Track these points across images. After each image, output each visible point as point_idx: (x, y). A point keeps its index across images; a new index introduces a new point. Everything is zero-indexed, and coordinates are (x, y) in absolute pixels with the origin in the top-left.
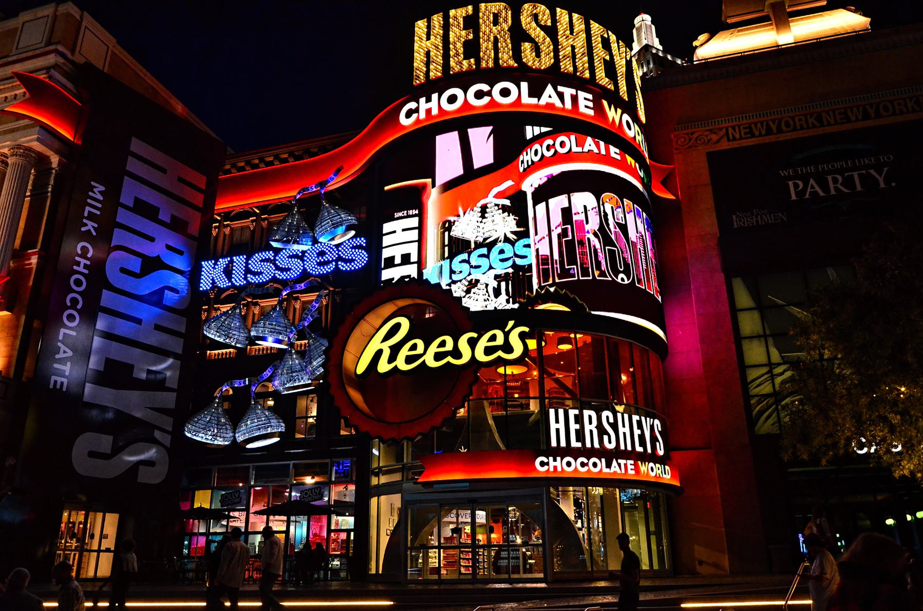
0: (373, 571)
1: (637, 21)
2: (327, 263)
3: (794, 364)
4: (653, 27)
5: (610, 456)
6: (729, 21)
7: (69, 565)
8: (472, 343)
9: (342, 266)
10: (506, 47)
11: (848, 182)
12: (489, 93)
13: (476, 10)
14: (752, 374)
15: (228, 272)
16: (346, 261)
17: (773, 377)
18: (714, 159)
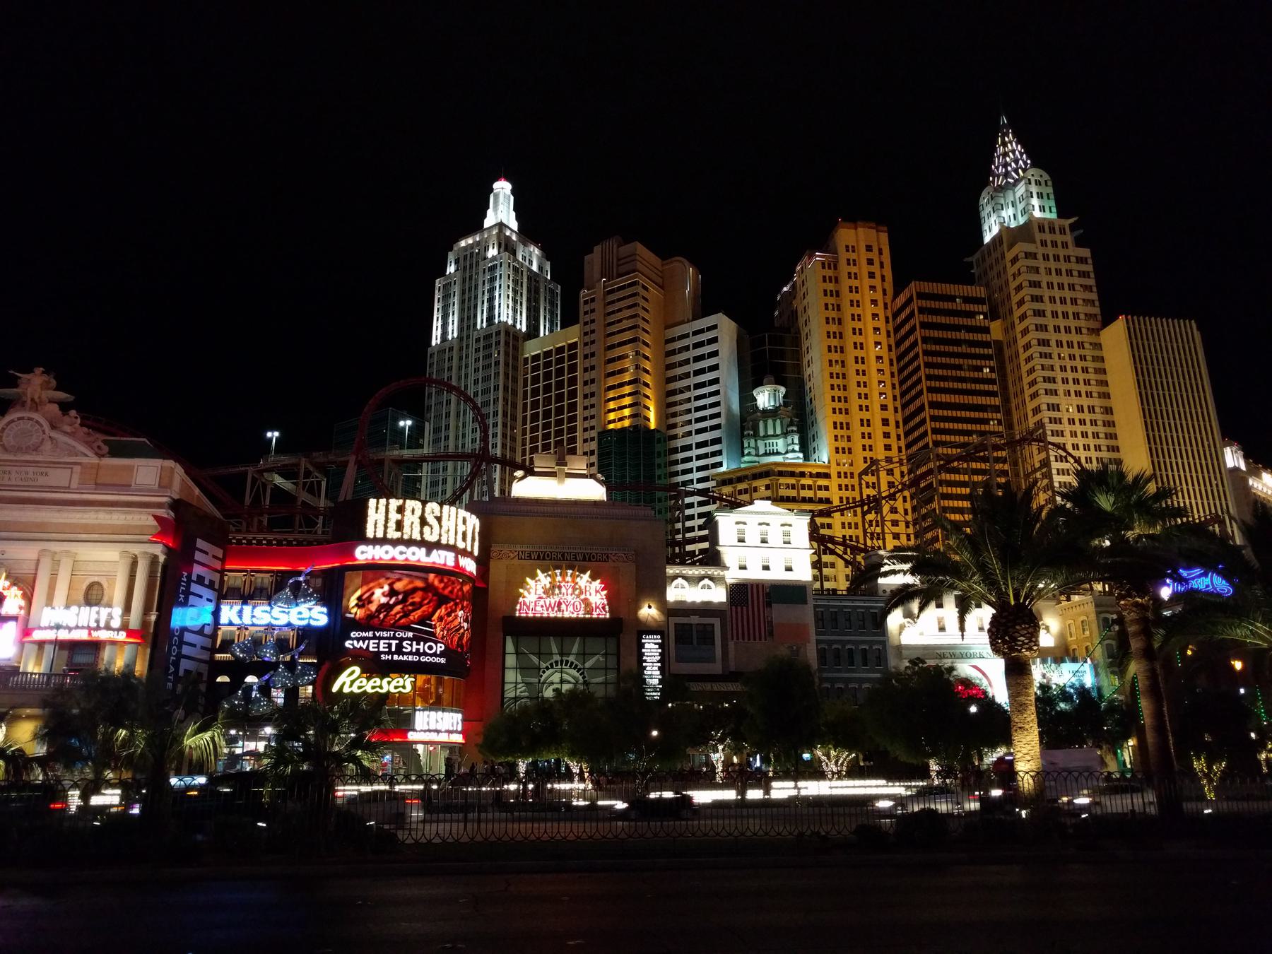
3: (527, 684)
4: (512, 198)
5: (438, 731)
6: (536, 470)
7: (897, 823)
8: (389, 683)
13: (404, 503)
14: (507, 687)
15: (240, 613)
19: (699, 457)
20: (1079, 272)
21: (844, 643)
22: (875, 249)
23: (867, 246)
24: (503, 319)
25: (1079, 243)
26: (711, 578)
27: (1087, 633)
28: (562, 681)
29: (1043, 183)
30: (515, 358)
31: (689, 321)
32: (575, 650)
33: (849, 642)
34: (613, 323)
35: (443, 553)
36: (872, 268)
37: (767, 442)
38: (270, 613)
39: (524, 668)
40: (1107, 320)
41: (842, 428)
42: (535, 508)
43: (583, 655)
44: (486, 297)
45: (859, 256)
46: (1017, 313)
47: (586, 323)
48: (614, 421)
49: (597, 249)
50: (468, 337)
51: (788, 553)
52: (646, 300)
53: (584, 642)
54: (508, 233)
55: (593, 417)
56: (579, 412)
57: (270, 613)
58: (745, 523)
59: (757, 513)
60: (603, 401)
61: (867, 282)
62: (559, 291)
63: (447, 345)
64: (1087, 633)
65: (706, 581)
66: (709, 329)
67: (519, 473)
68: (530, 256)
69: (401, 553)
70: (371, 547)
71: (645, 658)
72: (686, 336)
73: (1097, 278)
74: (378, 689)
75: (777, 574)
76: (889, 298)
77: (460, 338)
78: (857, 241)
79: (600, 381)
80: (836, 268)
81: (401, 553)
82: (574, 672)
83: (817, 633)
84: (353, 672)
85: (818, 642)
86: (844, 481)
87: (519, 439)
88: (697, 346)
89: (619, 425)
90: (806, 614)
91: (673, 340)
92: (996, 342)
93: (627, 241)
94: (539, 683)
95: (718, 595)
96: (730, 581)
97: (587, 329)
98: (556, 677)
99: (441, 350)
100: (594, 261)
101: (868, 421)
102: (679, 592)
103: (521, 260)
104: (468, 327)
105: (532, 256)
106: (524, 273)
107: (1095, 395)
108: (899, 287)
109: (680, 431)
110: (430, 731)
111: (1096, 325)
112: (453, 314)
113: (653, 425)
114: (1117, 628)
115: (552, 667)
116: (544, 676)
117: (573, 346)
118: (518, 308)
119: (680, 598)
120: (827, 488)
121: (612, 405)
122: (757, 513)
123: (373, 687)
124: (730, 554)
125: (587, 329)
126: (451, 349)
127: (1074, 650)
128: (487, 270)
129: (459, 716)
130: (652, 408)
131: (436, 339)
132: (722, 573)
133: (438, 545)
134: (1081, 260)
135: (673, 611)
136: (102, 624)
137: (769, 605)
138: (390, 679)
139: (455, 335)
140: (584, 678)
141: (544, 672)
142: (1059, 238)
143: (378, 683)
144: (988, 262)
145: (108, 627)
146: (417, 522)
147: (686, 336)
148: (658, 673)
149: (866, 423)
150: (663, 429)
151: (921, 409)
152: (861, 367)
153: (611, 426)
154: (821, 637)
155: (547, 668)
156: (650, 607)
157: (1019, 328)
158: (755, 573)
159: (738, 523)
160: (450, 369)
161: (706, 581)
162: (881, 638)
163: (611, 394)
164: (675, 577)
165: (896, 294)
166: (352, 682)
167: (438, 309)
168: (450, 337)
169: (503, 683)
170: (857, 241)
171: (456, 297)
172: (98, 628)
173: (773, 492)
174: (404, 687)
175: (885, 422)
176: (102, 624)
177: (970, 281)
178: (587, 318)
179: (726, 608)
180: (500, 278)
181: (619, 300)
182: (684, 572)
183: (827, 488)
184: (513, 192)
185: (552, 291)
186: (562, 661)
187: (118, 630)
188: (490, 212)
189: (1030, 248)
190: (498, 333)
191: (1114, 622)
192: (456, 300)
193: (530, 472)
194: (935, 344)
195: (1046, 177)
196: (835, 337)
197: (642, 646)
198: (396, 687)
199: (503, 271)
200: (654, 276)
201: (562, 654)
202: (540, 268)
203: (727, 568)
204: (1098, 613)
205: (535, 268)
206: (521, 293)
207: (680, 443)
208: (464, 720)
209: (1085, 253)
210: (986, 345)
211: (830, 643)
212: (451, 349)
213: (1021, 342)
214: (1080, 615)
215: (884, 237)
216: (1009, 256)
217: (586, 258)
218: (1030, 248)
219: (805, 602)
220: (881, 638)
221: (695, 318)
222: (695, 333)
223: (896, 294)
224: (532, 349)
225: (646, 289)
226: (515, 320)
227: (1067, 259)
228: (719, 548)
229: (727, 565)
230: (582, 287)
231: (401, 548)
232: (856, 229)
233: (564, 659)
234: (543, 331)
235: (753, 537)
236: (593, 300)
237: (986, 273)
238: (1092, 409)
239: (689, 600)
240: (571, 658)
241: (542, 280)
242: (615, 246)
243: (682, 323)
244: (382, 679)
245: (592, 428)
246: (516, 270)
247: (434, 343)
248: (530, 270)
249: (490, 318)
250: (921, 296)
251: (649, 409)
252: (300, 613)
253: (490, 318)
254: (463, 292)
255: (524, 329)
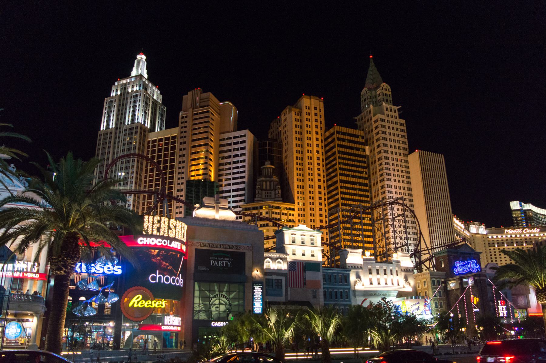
0: (330, 350)
1: (139, 56)
2: (110, 271)
3: (204, 304)
4: (146, 63)
5: (173, 326)
6: (205, 204)
8: (155, 303)
9: (115, 273)
10: (166, 231)
11: (223, 264)
12: (161, 242)
14: (195, 305)
16: (116, 271)
17: (199, 307)
18: (196, 250)
19: (234, 196)
20: (401, 129)
21: (333, 289)
22: (318, 109)
23: (315, 107)
24: (140, 121)
25: (401, 117)
26: (281, 259)
27: (426, 286)
28: (220, 304)
29: (388, 90)
30: (144, 140)
31: (232, 132)
32: (225, 289)
33: (341, 288)
34: (196, 129)
35: (176, 243)
36: (317, 118)
37: (267, 192)
38: (95, 267)
39: (204, 297)
40: (411, 151)
41: (301, 188)
42: (209, 223)
43: (229, 292)
44: (131, 110)
45: (311, 111)
46: (376, 144)
47: (182, 128)
48: (194, 176)
49: (190, 93)
50: (120, 128)
51: (313, 248)
52: (213, 120)
53: (220, 287)
54: (144, 80)
55: (183, 173)
56: (176, 170)
57: (95, 267)
58: (295, 235)
59: (301, 230)
60: (189, 166)
61: (314, 123)
62: (165, 110)
63: (109, 131)
64: (426, 286)
65: (279, 260)
66: (241, 136)
67: (197, 206)
68: (153, 92)
69: (159, 242)
70: (145, 238)
71: (255, 294)
72: (231, 138)
73: (407, 133)
74: (150, 306)
75: (308, 258)
76: (323, 132)
77: (116, 128)
78: (311, 105)
79: (188, 156)
80: (301, 115)
81: (159, 242)
82: (225, 300)
83: (324, 284)
84: (138, 297)
85: (324, 288)
86: (301, 212)
87: (143, 180)
88: (235, 143)
89: (197, 178)
90: (319, 276)
91: (224, 139)
92: (368, 155)
93: (204, 92)
94: (209, 304)
95: (284, 266)
96: (289, 260)
97: (183, 130)
98: (217, 302)
99: (106, 134)
100: (187, 99)
101: (312, 186)
102: (270, 264)
103: (149, 93)
104: (121, 123)
105: (156, 94)
106: (151, 100)
107: (405, 182)
108: (328, 126)
109: (224, 183)
110: (170, 325)
111: (407, 152)
112: (113, 116)
113: (212, 179)
114: (443, 285)
115: (215, 297)
116: (212, 301)
117: (174, 137)
118: (147, 116)
119: (279, 268)
120: (293, 215)
121: (193, 168)
122: (301, 230)
123: (148, 305)
124: (289, 249)
125: (183, 130)
126: (111, 133)
127: (420, 293)
128: (133, 97)
129: (180, 319)
130: (213, 171)
131: (103, 127)
132: (286, 256)
133: (175, 239)
134: (402, 124)
135: (267, 273)
136: (29, 270)
137: (304, 271)
138: (155, 301)
139: (114, 126)
140: (229, 302)
141: (212, 299)
142: (394, 114)
143: (150, 303)
144: (364, 120)
145: (31, 272)
146: (167, 228)
147: (231, 138)
148: (260, 301)
149: (311, 186)
150: (217, 181)
151: (336, 182)
152: (310, 161)
153: (193, 178)
154: (325, 286)
155: (213, 297)
156: (257, 271)
157: (377, 150)
158: (299, 257)
159: (292, 234)
160: (110, 142)
161: (279, 260)
162: (348, 287)
163: (193, 163)
164: (266, 258)
165: (326, 131)
166: (138, 302)
167: (105, 113)
168: (111, 127)
169: (194, 304)
170: (311, 105)
171: (115, 108)
172: (27, 272)
173: (269, 215)
174: (162, 305)
175: (320, 187)
176: (29, 270)
177: (355, 127)
178: (183, 125)
179: (287, 272)
180: (140, 101)
181: (200, 118)
182: (270, 255)
183: (293, 215)
184: (146, 60)
185: (162, 110)
186: (220, 294)
187: (36, 273)
188: (134, 69)
189: (382, 117)
190: (137, 128)
191: (443, 282)
192: (115, 109)
193: (202, 206)
194: (343, 154)
195: (389, 87)
196: (299, 147)
197: (254, 288)
198: (158, 305)
199: (141, 98)
200: (216, 109)
201: (220, 291)
202: (158, 98)
203: (289, 255)
204: (431, 278)
205: (155, 97)
206: (149, 110)
207: (224, 188)
208: (182, 321)
209: (403, 121)
210: (364, 156)
211: (328, 288)
212: (111, 133)
213: (377, 157)
214: (423, 279)
215: (322, 104)
216: (374, 119)
217: (184, 97)
218: (382, 117)
219: (319, 270)
220: (348, 287)
221: (235, 131)
222: (235, 138)
223: (326, 131)
224: (152, 137)
225: (213, 115)
226: (145, 122)
227: (396, 123)
228: (285, 245)
229: (288, 253)
230: (181, 110)
231: (160, 240)
232: (310, 99)
233: (221, 293)
234: (157, 129)
235: (298, 240)
236: (186, 117)
237: (363, 125)
238: (404, 188)
239: (272, 268)
240: (224, 293)
241: (159, 104)
242: (199, 93)
243: (228, 132)
244: (152, 301)
245: (183, 178)
246: (147, 98)
247: (102, 129)
248: (153, 99)
249: (133, 120)
250: (338, 132)
251: (211, 171)
252: (109, 268)
253: (133, 120)
254: (119, 106)
255: (149, 127)
